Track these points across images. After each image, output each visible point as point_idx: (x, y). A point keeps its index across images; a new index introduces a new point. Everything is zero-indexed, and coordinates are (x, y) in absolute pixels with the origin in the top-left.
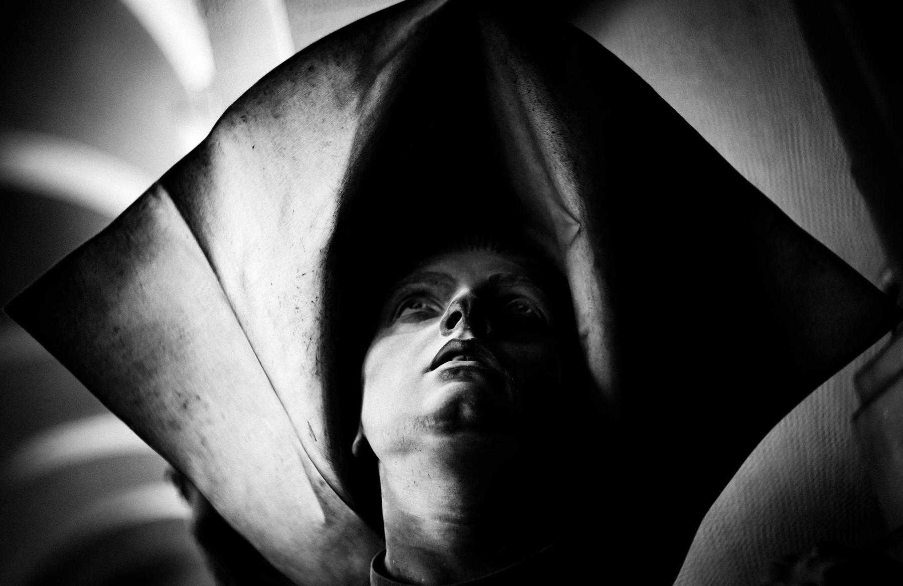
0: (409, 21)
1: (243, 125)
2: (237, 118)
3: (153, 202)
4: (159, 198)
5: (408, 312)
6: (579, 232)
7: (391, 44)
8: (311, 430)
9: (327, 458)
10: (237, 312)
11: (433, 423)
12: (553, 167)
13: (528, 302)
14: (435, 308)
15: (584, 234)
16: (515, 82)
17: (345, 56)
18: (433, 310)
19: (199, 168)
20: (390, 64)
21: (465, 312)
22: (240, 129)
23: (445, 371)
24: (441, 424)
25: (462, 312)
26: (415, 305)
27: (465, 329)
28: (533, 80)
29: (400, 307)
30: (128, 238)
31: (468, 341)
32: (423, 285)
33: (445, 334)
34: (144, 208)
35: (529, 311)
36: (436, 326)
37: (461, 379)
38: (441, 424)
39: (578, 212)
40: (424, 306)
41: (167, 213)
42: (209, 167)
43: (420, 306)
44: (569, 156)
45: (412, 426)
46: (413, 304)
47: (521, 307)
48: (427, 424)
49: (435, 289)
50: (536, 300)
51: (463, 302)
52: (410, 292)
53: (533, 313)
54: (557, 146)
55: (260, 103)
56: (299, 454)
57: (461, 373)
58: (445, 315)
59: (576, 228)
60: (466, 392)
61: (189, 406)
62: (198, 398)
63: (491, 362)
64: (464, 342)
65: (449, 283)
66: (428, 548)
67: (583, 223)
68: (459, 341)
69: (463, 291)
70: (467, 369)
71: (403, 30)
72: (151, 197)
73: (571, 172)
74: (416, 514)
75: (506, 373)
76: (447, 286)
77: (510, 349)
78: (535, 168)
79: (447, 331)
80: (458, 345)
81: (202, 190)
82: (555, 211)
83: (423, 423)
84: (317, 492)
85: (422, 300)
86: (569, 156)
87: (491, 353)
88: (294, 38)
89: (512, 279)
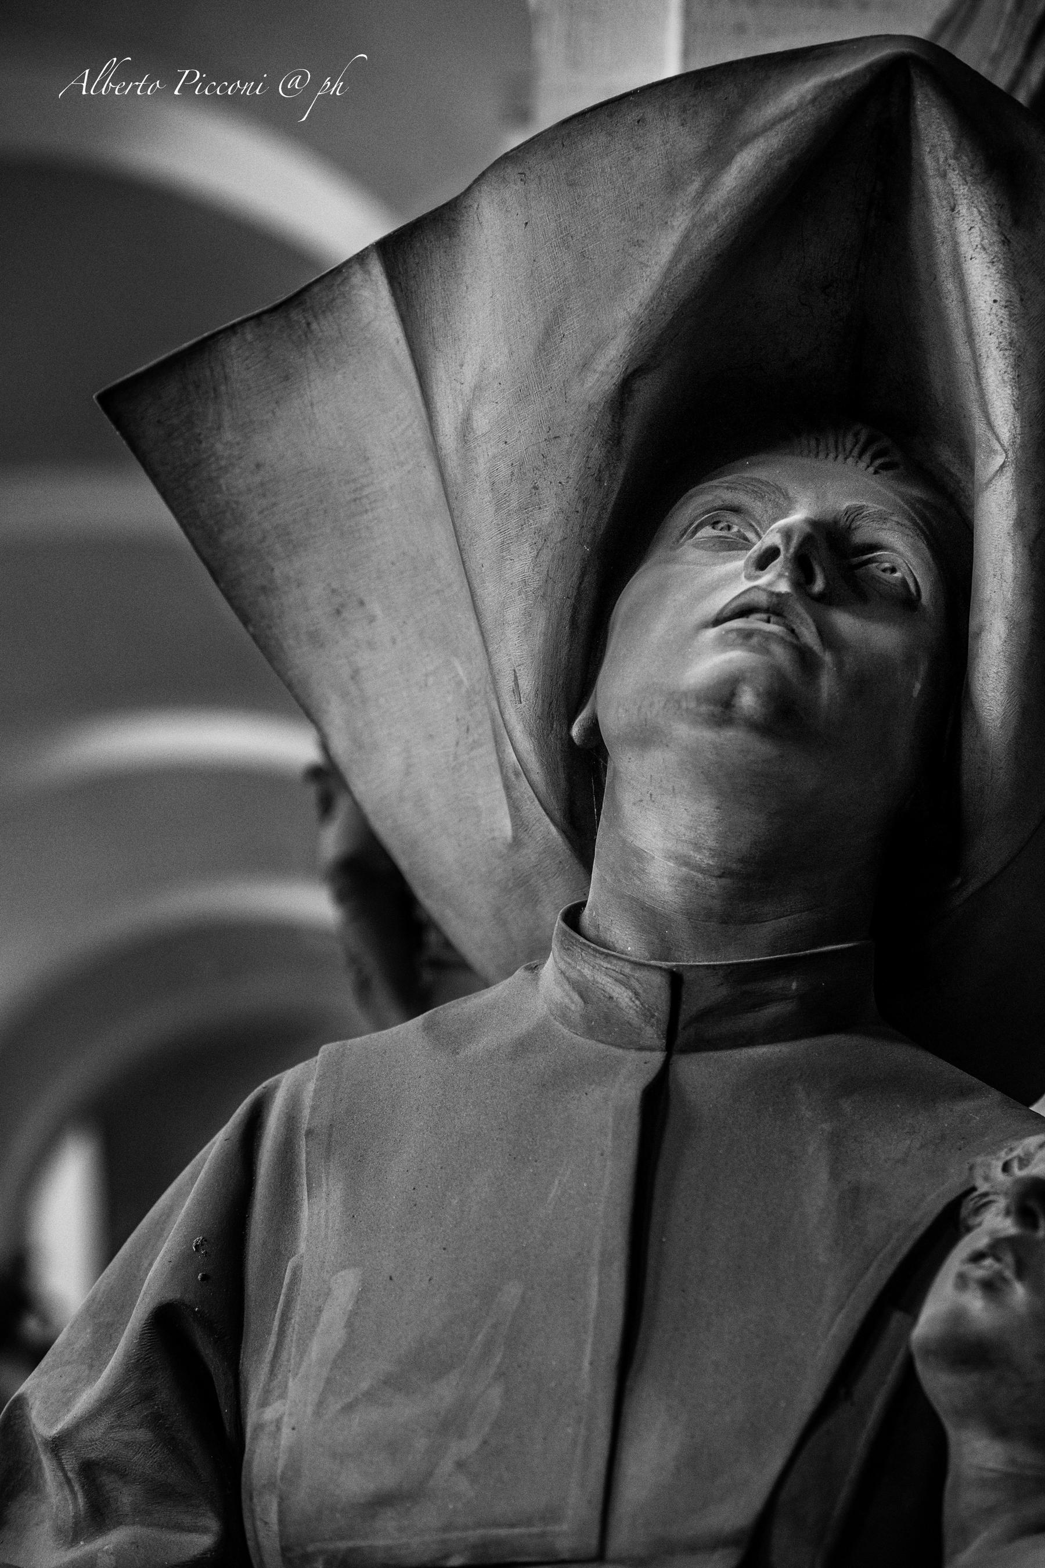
0: (807, 80)
1: (519, 186)
2: (511, 172)
3: (357, 277)
4: (368, 272)
5: (707, 532)
6: (1002, 467)
7: (771, 110)
8: (517, 684)
9: (531, 734)
10: (446, 476)
11: (692, 705)
12: (984, 356)
13: (900, 561)
14: (751, 535)
15: (1009, 472)
16: (953, 210)
17: (696, 113)
18: (746, 539)
19: (438, 239)
20: (762, 140)
21: (787, 550)
22: (512, 191)
23: (732, 631)
24: (704, 709)
25: (782, 548)
26: (721, 525)
27: (780, 576)
28: (980, 212)
29: (696, 523)
30: (308, 324)
31: (779, 595)
32: (741, 498)
33: (749, 578)
34: (343, 283)
35: (898, 574)
36: (739, 563)
37: (752, 649)
38: (704, 709)
39: (1008, 434)
40: (735, 529)
41: (374, 298)
42: (456, 240)
43: (729, 528)
44: (1011, 343)
45: (662, 704)
46: (718, 522)
47: (887, 565)
48: (684, 705)
49: (757, 507)
50: (914, 562)
51: (787, 534)
52: (718, 503)
53: (904, 582)
54: (996, 323)
55: (552, 157)
56: (493, 721)
57: (755, 640)
58: (759, 546)
59: (1000, 460)
60: (753, 670)
61: (345, 614)
62: (362, 603)
63: (809, 636)
64: (772, 594)
65: (781, 501)
66: (649, 902)
67: (1010, 454)
68: (764, 590)
69: (798, 516)
70: (768, 636)
71: (797, 93)
72: (357, 267)
73: (1009, 369)
74: (643, 846)
75: (827, 658)
76: (777, 505)
77: (845, 622)
78: (963, 351)
79: (753, 571)
80: (762, 599)
81: (437, 274)
82: (980, 428)
83: (678, 702)
84: (508, 787)
85: (734, 519)
86: (1011, 343)
87: (810, 621)
88: (686, 53)
89: (883, 518)
